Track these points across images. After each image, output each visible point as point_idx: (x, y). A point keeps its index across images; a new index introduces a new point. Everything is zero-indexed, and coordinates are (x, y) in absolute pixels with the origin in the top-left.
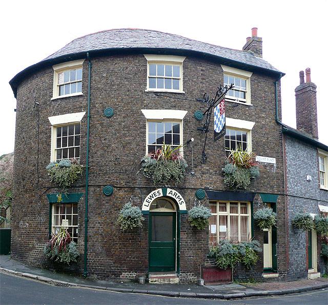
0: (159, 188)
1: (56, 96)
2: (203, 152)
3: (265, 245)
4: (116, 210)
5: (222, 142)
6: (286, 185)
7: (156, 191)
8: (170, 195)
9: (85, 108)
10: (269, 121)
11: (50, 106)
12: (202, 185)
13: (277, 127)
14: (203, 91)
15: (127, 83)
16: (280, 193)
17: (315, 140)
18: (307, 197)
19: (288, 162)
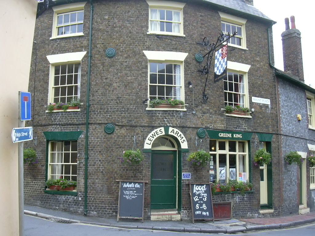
0: (161, 126)
1: (54, 36)
2: (204, 93)
3: (261, 182)
4: (118, 148)
5: (221, 83)
6: (280, 125)
7: (158, 129)
8: (172, 134)
9: (86, 48)
10: (263, 65)
11: (49, 45)
12: (202, 124)
13: (271, 71)
14: (202, 35)
15: (128, 25)
16: (274, 132)
17: (302, 82)
18: (297, 136)
19: (281, 104)
